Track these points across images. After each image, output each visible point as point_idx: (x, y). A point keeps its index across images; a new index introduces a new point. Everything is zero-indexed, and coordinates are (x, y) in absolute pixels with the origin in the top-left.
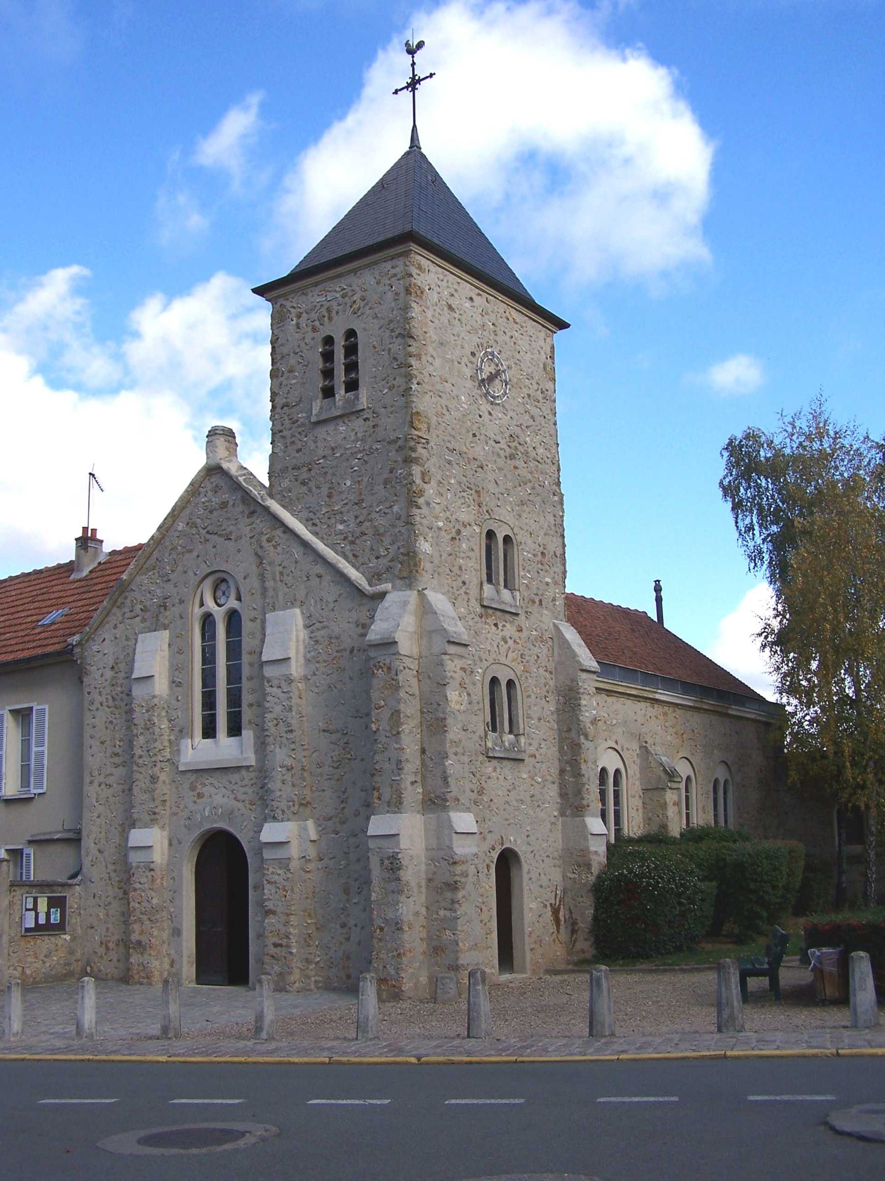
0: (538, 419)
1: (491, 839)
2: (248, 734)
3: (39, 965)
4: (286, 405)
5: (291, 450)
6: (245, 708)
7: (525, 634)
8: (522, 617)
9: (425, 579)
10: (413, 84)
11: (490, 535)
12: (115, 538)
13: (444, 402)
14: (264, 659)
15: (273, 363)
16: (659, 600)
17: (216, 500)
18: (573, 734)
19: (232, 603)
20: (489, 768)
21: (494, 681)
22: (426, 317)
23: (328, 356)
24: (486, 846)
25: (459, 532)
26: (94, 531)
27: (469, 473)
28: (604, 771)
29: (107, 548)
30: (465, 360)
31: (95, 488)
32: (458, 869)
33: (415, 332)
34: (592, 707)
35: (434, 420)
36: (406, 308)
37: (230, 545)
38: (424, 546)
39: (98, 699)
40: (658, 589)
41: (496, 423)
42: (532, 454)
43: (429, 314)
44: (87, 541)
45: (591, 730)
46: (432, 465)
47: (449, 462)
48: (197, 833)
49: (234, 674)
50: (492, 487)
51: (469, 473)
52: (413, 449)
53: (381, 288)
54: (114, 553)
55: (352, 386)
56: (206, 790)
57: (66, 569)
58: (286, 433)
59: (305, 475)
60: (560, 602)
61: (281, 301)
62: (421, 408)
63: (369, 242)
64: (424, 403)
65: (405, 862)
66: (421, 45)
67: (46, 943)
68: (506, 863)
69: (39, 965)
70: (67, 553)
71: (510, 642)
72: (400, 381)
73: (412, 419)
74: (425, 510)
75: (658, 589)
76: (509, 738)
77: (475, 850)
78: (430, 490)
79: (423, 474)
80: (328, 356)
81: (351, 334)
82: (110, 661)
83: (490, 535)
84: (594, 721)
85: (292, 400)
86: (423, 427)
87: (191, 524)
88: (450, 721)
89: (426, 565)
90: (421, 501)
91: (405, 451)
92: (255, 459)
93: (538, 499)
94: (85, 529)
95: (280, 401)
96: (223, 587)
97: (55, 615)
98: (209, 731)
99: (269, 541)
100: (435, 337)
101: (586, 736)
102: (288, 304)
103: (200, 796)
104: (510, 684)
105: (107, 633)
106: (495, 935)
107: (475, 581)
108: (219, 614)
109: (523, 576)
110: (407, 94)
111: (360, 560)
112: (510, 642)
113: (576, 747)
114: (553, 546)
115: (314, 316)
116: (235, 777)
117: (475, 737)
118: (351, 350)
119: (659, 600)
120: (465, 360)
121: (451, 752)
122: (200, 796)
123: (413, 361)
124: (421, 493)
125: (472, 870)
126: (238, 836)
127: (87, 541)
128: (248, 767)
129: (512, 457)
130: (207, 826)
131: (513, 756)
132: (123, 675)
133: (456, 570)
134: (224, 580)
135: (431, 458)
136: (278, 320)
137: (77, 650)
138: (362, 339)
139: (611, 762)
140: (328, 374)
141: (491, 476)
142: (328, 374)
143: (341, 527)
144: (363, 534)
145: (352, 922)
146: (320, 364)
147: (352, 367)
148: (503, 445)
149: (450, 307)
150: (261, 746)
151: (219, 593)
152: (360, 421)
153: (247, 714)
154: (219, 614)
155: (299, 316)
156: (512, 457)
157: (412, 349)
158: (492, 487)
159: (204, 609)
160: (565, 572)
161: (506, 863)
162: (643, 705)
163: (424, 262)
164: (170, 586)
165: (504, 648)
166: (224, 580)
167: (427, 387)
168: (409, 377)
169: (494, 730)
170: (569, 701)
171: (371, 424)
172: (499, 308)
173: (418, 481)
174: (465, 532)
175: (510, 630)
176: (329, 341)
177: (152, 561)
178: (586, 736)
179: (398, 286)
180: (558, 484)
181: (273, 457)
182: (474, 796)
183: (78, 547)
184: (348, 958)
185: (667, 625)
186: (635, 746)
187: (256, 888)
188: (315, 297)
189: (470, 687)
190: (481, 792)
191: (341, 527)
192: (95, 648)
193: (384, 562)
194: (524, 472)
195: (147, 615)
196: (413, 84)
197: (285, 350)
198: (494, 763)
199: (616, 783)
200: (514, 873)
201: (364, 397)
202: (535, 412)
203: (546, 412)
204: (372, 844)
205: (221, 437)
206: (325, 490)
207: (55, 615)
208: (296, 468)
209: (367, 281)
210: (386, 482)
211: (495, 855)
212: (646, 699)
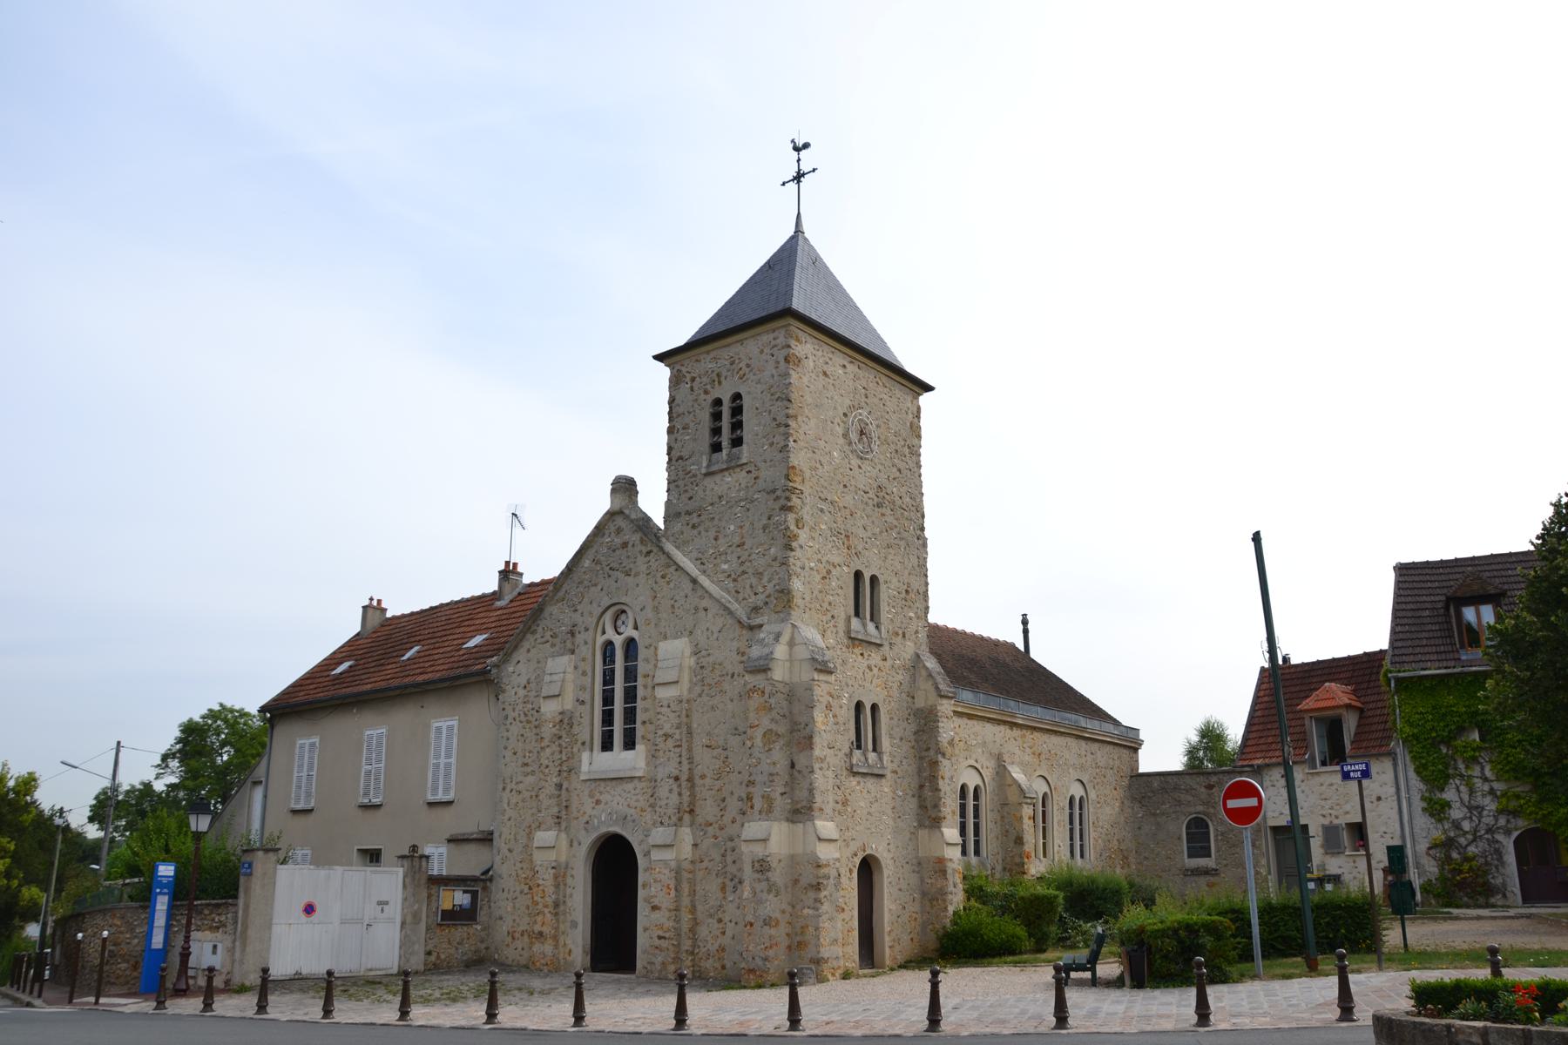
0: (905, 472)
1: (854, 846)
2: (640, 747)
3: (452, 951)
4: (681, 458)
5: (684, 497)
6: (638, 725)
7: (889, 662)
8: (886, 648)
9: (795, 614)
10: (798, 177)
11: (858, 575)
12: (531, 576)
13: (817, 457)
14: (657, 680)
15: (670, 420)
16: (1026, 632)
17: (618, 541)
18: (932, 753)
19: (630, 632)
20: (854, 781)
21: (859, 706)
22: (804, 381)
23: (717, 416)
24: (848, 852)
25: (829, 572)
26: (515, 565)
27: (840, 520)
28: (963, 788)
29: (526, 580)
30: (837, 420)
31: (517, 529)
32: (823, 871)
33: (793, 397)
34: (949, 728)
35: (807, 474)
36: (787, 375)
37: (630, 580)
38: (797, 585)
39: (512, 715)
40: (1025, 622)
41: (865, 476)
42: (899, 502)
43: (805, 380)
44: (509, 573)
45: (949, 751)
46: (806, 513)
47: (822, 510)
48: (594, 836)
49: (630, 695)
50: (861, 533)
51: (840, 520)
52: (788, 499)
53: (764, 357)
54: (532, 585)
55: (737, 442)
56: (605, 798)
57: (495, 596)
58: (680, 483)
59: (695, 520)
60: (923, 635)
61: (678, 367)
62: (795, 463)
63: (755, 316)
64: (799, 458)
65: (774, 865)
66: (806, 146)
67: (459, 932)
68: (868, 869)
69: (452, 951)
70: (491, 585)
71: (875, 670)
72: (779, 439)
73: (789, 472)
74: (798, 553)
75: (1025, 622)
76: (872, 756)
77: (837, 855)
78: (803, 535)
79: (797, 521)
80: (717, 416)
81: (737, 396)
82: (524, 682)
83: (858, 575)
84: (951, 743)
85: (685, 454)
86: (798, 479)
87: (596, 562)
88: (817, 740)
89: (797, 601)
90: (794, 544)
91: (783, 497)
92: (653, 502)
93: (902, 543)
94: (507, 563)
95: (675, 454)
96: (623, 617)
97: (478, 640)
98: (607, 745)
99: (663, 577)
100: (810, 400)
101: (944, 755)
102: (684, 370)
103: (598, 802)
104: (874, 707)
105: (521, 655)
106: (856, 933)
107: (843, 616)
108: (618, 641)
109: (885, 613)
110: (793, 185)
111: (741, 596)
112: (875, 670)
113: (934, 764)
114: (916, 584)
115: (705, 379)
116: (630, 786)
117: (841, 754)
118: (737, 411)
119: (1026, 632)
120: (837, 420)
121: (816, 766)
122: (598, 802)
123: (792, 423)
124: (796, 537)
125: (833, 873)
126: (630, 839)
127: (509, 573)
128: (640, 778)
129: (879, 505)
130: (604, 830)
131: (876, 771)
132: (533, 693)
133: (826, 605)
134: (624, 612)
135: (806, 506)
136: (675, 382)
137: (494, 671)
138: (746, 403)
139: (972, 781)
140: (716, 431)
141: (860, 523)
142: (716, 431)
143: (725, 567)
144: (744, 572)
145: (727, 919)
146: (745, 417)
147: (737, 426)
148: (871, 495)
149: (825, 374)
150: (653, 756)
151: (619, 623)
152: (744, 473)
153: (640, 730)
154: (618, 641)
155: (693, 380)
156: (879, 505)
157: (790, 412)
158: (861, 533)
159: (605, 637)
160: (927, 608)
161: (868, 869)
162: (1002, 728)
163: (800, 333)
164: (578, 615)
165: (869, 675)
166: (624, 612)
167: (801, 444)
168: (787, 435)
169: (859, 747)
170: (925, 724)
171: (752, 476)
172: (868, 376)
173: (793, 527)
174: (834, 572)
175: (875, 658)
176: (718, 402)
177: (561, 594)
178: (944, 755)
179: (781, 355)
180: (923, 529)
181: (668, 504)
182: (839, 806)
183: (501, 581)
184: (723, 950)
185: (1033, 655)
186: (992, 764)
187: (644, 886)
188: (706, 362)
189: (836, 710)
190: (845, 803)
191: (725, 567)
192: (511, 669)
193: (762, 597)
194: (890, 519)
195: (557, 641)
196: (798, 177)
197: (681, 410)
198: (858, 778)
199: (976, 797)
200: (875, 878)
201: (745, 452)
202: (902, 465)
203: (912, 465)
204: (744, 848)
205: (625, 487)
206: (712, 534)
207: (478, 640)
208: (688, 513)
209: (751, 348)
210: (765, 528)
211: (857, 861)
212: (1005, 723)
